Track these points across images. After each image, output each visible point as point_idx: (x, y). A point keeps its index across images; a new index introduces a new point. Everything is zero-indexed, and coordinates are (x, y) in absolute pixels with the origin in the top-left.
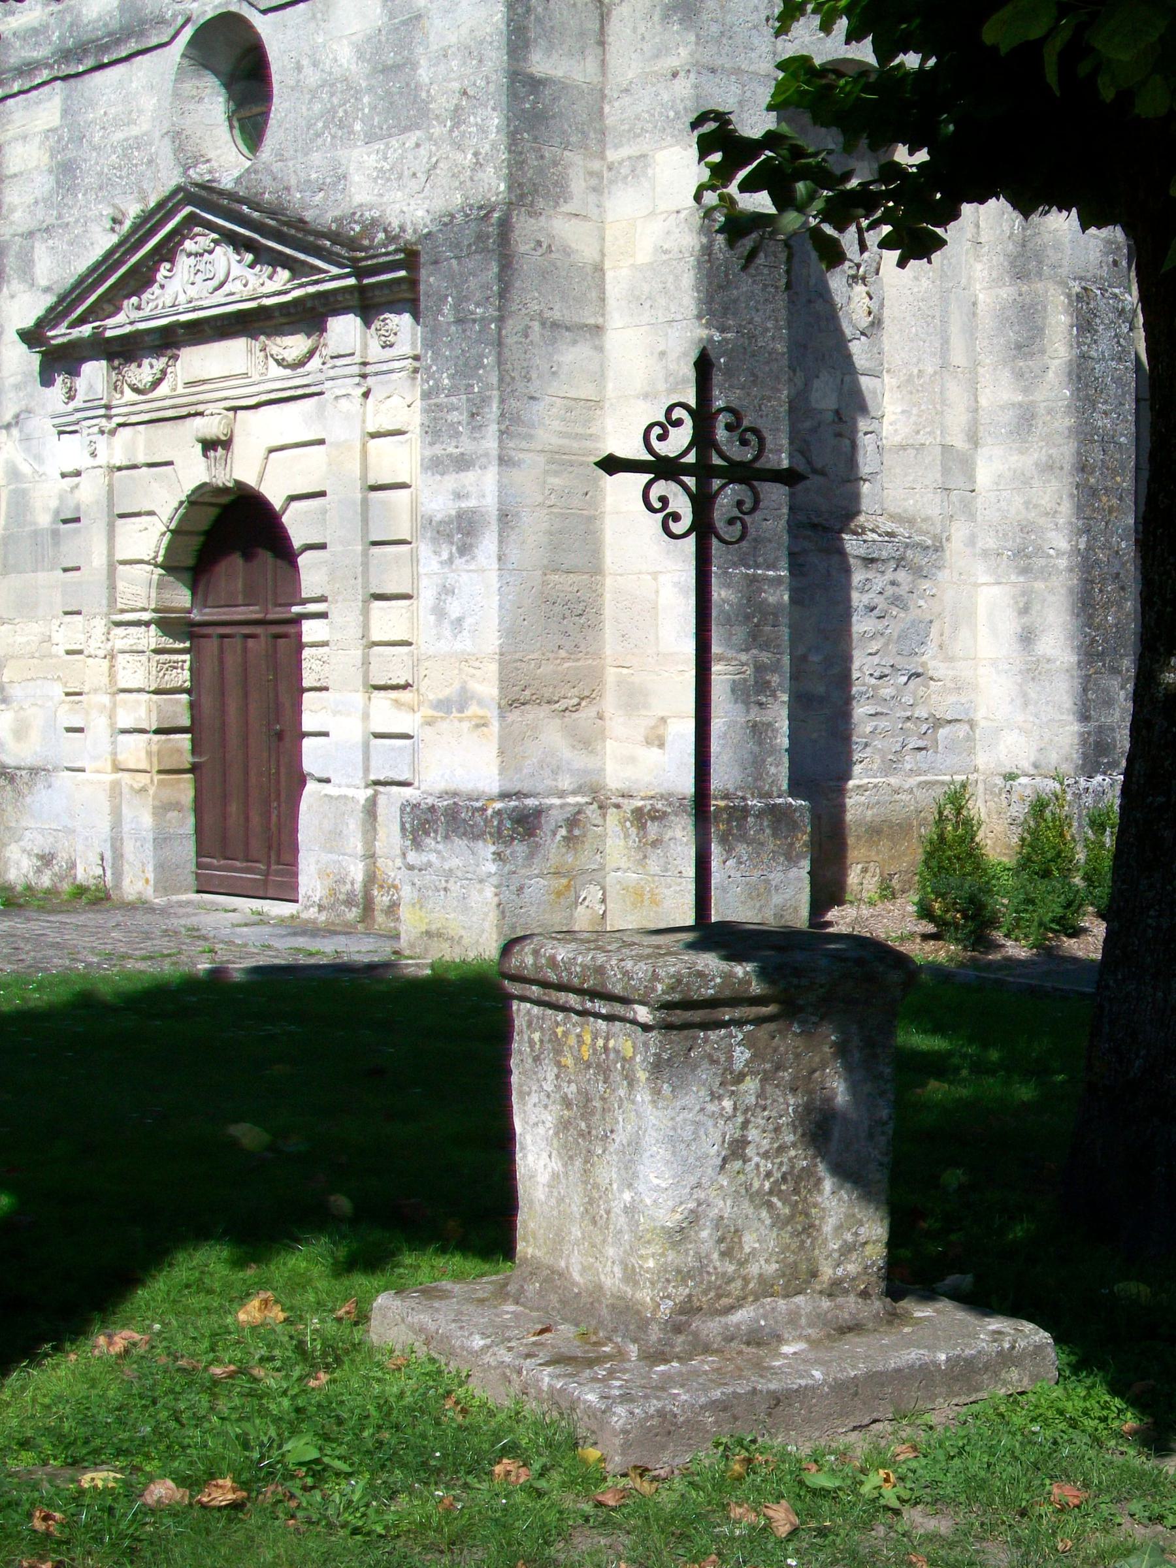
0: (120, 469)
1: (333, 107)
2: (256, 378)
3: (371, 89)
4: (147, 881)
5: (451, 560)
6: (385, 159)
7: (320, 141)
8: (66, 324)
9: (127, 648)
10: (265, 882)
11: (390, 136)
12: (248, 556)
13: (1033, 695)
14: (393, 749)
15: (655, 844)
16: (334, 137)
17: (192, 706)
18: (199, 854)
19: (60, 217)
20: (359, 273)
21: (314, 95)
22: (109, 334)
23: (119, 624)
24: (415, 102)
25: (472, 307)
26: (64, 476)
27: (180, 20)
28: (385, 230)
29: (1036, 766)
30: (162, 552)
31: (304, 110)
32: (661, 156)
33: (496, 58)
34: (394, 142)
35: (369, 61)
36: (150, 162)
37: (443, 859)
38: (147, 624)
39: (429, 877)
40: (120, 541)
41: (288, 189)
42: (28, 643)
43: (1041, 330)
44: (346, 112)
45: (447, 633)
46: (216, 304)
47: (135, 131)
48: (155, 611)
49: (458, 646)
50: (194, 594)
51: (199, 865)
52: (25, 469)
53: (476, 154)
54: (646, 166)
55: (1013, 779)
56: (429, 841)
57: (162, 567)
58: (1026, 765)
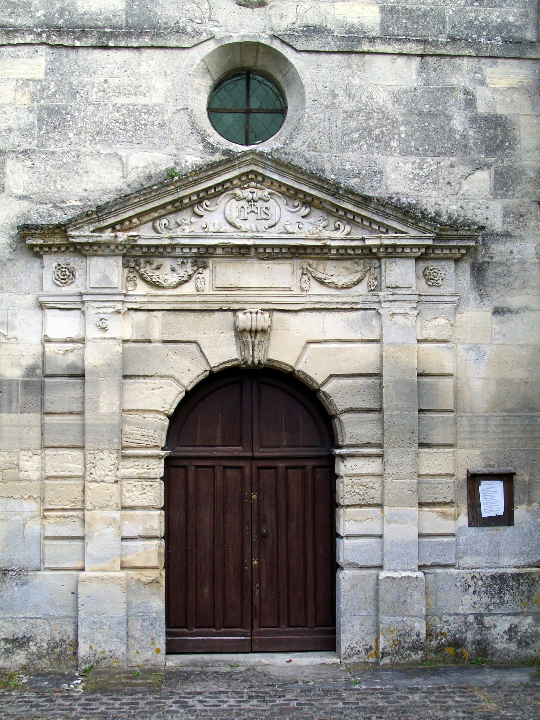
1: (369, 126)
3: (407, 123)
6: (422, 169)
7: (355, 146)
11: (426, 155)
14: (440, 544)
16: (369, 146)
18: (168, 625)
21: (349, 115)
22: (140, 242)
24: (449, 138)
27: (204, 36)
31: (339, 123)
34: (429, 159)
35: (405, 105)
44: (382, 132)
46: (272, 237)
47: (142, 101)
51: (168, 634)
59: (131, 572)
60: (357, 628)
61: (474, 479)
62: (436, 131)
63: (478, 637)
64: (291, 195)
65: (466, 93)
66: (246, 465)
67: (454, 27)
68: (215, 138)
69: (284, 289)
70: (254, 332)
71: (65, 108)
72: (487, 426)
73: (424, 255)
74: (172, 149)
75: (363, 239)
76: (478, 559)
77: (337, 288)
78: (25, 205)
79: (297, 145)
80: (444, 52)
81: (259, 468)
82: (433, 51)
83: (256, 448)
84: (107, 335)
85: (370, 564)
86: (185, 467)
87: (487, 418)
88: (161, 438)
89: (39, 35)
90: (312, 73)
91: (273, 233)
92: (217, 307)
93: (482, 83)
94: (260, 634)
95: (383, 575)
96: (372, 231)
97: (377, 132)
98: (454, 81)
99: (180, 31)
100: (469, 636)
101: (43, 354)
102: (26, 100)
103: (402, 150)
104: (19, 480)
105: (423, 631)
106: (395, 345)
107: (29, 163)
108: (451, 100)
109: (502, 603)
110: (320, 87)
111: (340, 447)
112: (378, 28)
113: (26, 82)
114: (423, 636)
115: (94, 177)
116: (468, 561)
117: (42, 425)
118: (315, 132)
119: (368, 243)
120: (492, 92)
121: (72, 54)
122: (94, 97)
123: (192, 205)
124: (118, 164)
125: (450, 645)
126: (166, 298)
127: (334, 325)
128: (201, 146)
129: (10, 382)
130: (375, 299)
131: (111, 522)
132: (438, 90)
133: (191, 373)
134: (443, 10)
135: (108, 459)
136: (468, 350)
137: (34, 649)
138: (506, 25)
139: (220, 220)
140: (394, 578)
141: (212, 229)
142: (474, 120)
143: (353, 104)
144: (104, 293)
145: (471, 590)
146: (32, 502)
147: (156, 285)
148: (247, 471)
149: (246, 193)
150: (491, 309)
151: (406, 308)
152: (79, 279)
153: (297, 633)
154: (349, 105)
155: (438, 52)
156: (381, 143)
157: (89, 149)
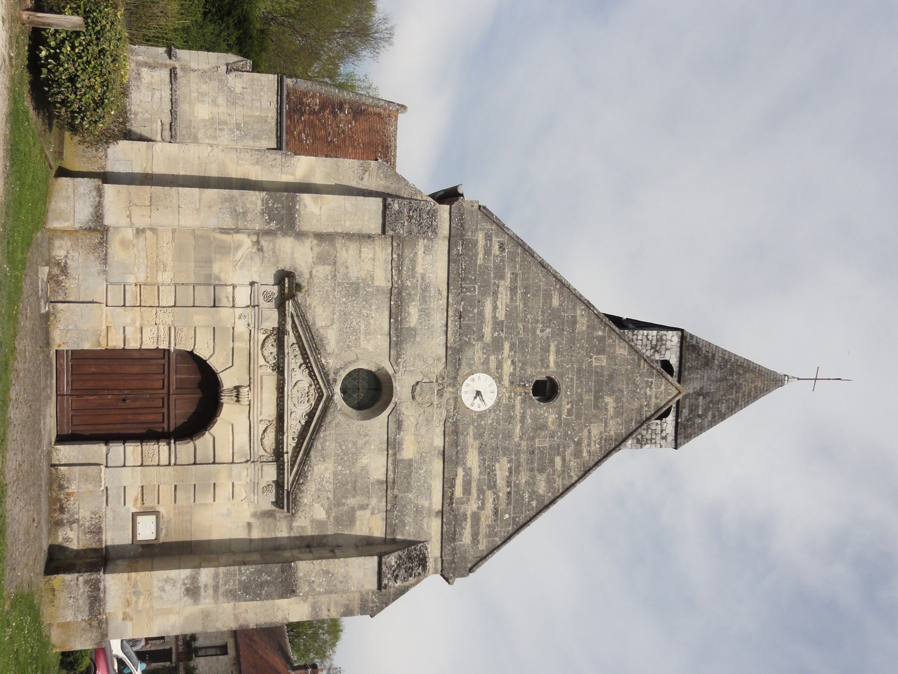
5: (184, 584)
15: (90, 624)
18: (72, 351)
19: (339, 284)
21: (355, 444)
23: (170, 329)
34: (331, 486)
36: (349, 346)
41: (325, 430)
46: (288, 404)
47: (362, 337)
49: (155, 589)
51: (67, 351)
52: (239, 255)
56: (87, 589)
59: (105, 331)
60: (72, 454)
63: (65, 521)
64: (311, 415)
65: (367, 505)
66: (166, 390)
68: (343, 374)
69: (261, 411)
70: (238, 396)
73: (279, 484)
74: (336, 351)
76: (111, 518)
77: (262, 439)
78: (307, 276)
79: (340, 417)
81: (163, 398)
84: (237, 320)
86: (164, 358)
87: (191, 521)
88: (180, 347)
90: (379, 424)
91: (291, 406)
93: (373, 513)
94: (67, 400)
95: (103, 467)
96: (292, 457)
99: (398, 356)
100: (65, 516)
101: (226, 285)
104: (157, 271)
105: (70, 491)
107: (329, 277)
109: (85, 533)
113: (372, 277)
114: (67, 490)
116: (110, 515)
117: (187, 284)
123: (305, 363)
124: (328, 324)
125: (61, 506)
126: (257, 350)
127: (242, 439)
129: (211, 267)
133: (216, 363)
139: (298, 378)
142: (353, 509)
144: (259, 319)
148: (162, 392)
149: (312, 392)
152: (267, 305)
153: (68, 420)
154: (360, 442)
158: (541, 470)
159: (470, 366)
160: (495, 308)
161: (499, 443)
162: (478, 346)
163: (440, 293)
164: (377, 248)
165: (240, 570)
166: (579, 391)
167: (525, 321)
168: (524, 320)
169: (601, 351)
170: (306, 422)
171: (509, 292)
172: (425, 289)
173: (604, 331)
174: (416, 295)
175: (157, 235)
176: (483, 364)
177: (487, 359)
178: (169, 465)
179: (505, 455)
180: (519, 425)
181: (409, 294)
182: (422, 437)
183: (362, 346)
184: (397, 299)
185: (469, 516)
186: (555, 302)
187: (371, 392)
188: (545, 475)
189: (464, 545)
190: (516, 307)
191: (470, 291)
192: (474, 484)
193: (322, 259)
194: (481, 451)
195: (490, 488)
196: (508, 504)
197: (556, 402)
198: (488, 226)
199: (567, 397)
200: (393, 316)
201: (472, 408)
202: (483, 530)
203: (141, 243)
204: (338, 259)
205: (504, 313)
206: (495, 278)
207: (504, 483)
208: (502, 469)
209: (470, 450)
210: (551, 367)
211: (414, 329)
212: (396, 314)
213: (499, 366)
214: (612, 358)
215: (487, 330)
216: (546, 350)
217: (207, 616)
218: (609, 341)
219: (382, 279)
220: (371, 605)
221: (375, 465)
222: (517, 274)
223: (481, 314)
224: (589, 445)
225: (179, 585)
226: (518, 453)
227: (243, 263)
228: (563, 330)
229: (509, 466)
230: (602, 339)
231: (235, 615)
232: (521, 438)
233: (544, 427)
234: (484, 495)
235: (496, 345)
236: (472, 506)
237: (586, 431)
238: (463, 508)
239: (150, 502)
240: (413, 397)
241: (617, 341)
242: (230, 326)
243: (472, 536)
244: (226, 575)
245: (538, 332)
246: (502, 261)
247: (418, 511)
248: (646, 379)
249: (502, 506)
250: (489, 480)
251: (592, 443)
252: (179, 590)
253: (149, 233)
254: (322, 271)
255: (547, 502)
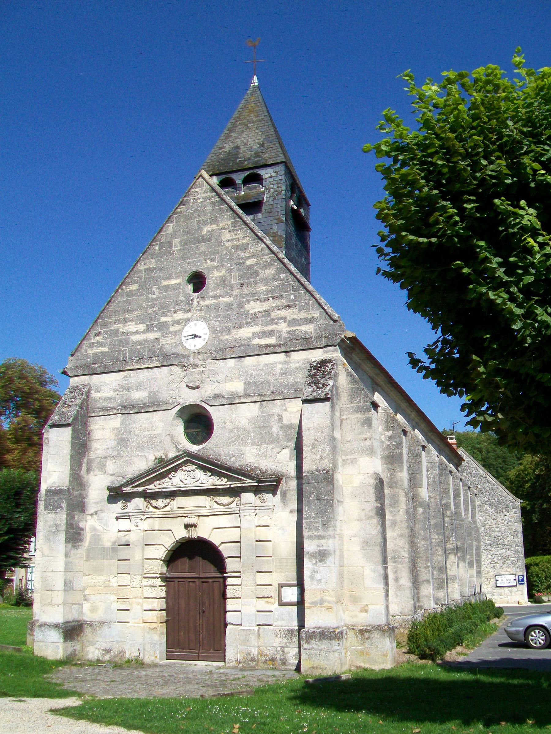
0: (146, 531)
1: (239, 435)
2: (209, 508)
3: (254, 432)
4: (156, 657)
5: (316, 563)
6: (260, 451)
7: (233, 444)
8: (130, 487)
9: (149, 585)
10: (198, 656)
12: (191, 558)
13: (399, 594)
14: (266, 615)
15: (367, 639)
16: (239, 443)
17: (166, 602)
18: (167, 647)
19: (119, 454)
20: (259, 482)
21: (231, 431)
22: (148, 491)
23: (145, 578)
25: (323, 496)
26: (119, 531)
27: (176, 404)
28: (260, 470)
29: (401, 613)
30: (164, 556)
31: (227, 434)
32: (361, 459)
33: (326, 432)
34: (263, 446)
36: (161, 442)
37: (319, 646)
38: (158, 578)
39: (312, 651)
40: (145, 552)
41: (220, 455)
42: (99, 582)
43: (397, 501)
45: (315, 583)
46: (196, 486)
48: (160, 574)
50: (167, 569)
51: (167, 651)
52: (99, 528)
53: (321, 456)
54: (356, 461)
55: (395, 616)
56: (313, 641)
57: (162, 561)
58: (398, 613)
60: (232, 651)
61: (281, 586)
62: (266, 433)
63: (282, 657)
65: (279, 415)
67: (274, 387)
71: (127, 438)
72: (287, 563)
73: (256, 490)
75: (230, 485)
76: (284, 622)
77: (223, 505)
78: (113, 477)
80: (269, 399)
81: (203, 582)
82: (264, 399)
83: (201, 573)
85: (237, 623)
89: (118, 410)
90: (217, 414)
91: (197, 484)
92: (178, 515)
93: (286, 410)
94: (202, 653)
97: (242, 437)
98: (274, 411)
99: (167, 403)
100: (278, 657)
102: (114, 436)
103: (252, 444)
104: (109, 586)
105: (256, 653)
106: (245, 529)
107: (114, 461)
108: (273, 419)
110: (220, 420)
111: (226, 573)
112: (243, 392)
113: (114, 429)
115: (136, 465)
116: (279, 623)
118: (218, 439)
119: (232, 486)
120: (290, 414)
121: (129, 416)
122: (137, 433)
124: (145, 459)
125: (270, 660)
126: (160, 513)
128: (175, 449)
130: (238, 509)
131: (139, 604)
132: (267, 415)
134: (269, 380)
135: (138, 578)
136: (279, 529)
137: (112, 654)
138: (297, 383)
139: (178, 480)
140: (244, 630)
141: (174, 484)
142: (281, 427)
143: (233, 425)
144: (137, 512)
145: (279, 636)
146: (114, 595)
147: (156, 508)
148: (197, 583)
150: (289, 510)
151: (250, 512)
154: (230, 426)
155: (267, 399)
156: (243, 441)
157: (135, 454)
158: (256, 274)
159: (176, 346)
160: (137, 333)
161: (234, 313)
162: (163, 341)
163: (126, 376)
164: (96, 427)
165: (307, 518)
166: (197, 256)
167: (147, 308)
168: (146, 309)
169: (170, 244)
170: (209, 471)
171: (128, 324)
172: (124, 388)
173: (155, 245)
174: (126, 394)
175: (87, 586)
176: (175, 336)
177: (172, 333)
178: (240, 577)
179: (243, 307)
180: (221, 299)
181: (126, 399)
182: (228, 378)
183: (160, 432)
184: (129, 409)
185: (291, 329)
186: (134, 287)
187: (198, 422)
188: (260, 271)
189: (315, 330)
190: (137, 317)
191: (125, 354)
192: (266, 329)
193: (103, 468)
194: (240, 327)
195: (269, 315)
196: (282, 297)
197: (205, 272)
198: (84, 347)
199: (201, 264)
200: (140, 410)
201: (207, 339)
202: (304, 315)
203: (92, 597)
204: (103, 456)
205: (141, 325)
206: (117, 336)
207: (265, 304)
208: (254, 307)
209: (239, 336)
210: (179, 281)
211: (150, 393)
212: (140, 408)
213: (177, 322)
214: (175, 234)
215: (152, 336)
216: (167, 287)
217: (367, 543)
218: (163, 240)
219: (116, 422)
220: (362, 403)
221: (248, 412)
222: (116, 320)
223: (141, 343)
224: (238, 239)
225: (317, 568)
226: (242, 296)
227: (104, 525)
228: (154, 277)
229: (252, 302)
230: (161, 246)
231: (366, 519)
232: (231, 296)
233: (223, 279)
234: (275, 319)
235: (163, 327)
236: (283, 327)
237: (227, 244)
238: (284, 335)
239: (272, 591)
240: (197, 387)
241: (162, 234)
242: (142, 534)
243: (307, 324)
244: (310, 530)
245: (155, 296)
246: (105, 333)
247: (285, 373)
248: (191, 204)
249: (284, 302)
250: (263, 316)
251: (237, 237)
252: (321, 567)
253: (86, 592)
254: (111, 466)
255: (282, 266)
